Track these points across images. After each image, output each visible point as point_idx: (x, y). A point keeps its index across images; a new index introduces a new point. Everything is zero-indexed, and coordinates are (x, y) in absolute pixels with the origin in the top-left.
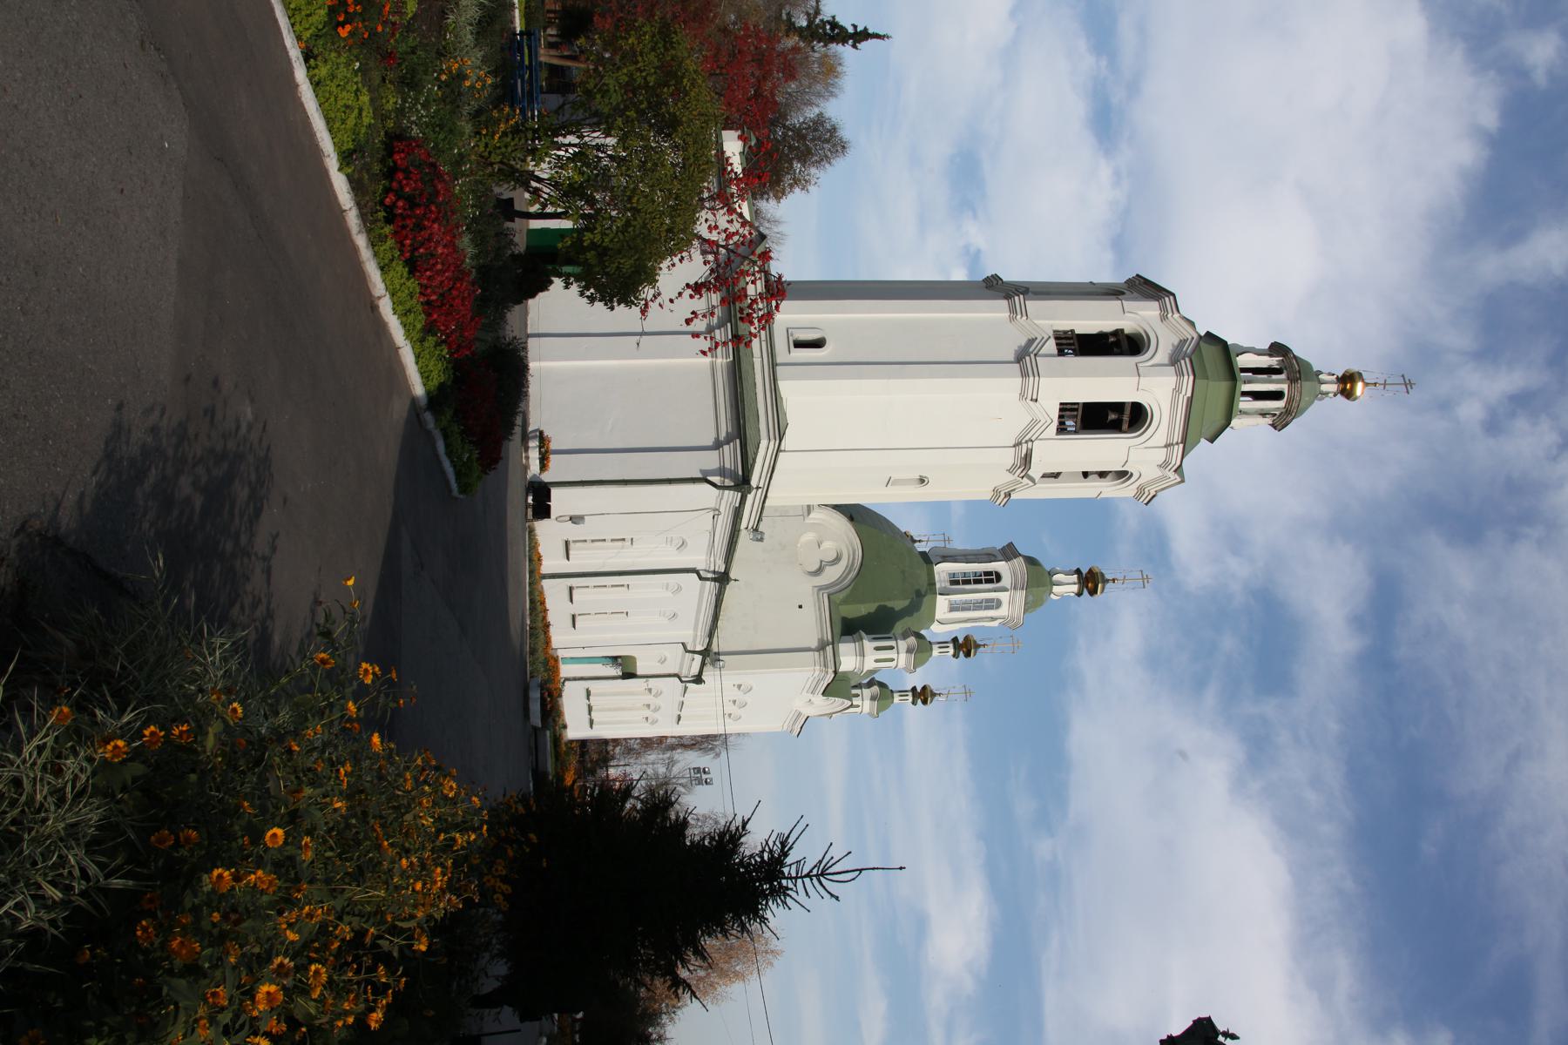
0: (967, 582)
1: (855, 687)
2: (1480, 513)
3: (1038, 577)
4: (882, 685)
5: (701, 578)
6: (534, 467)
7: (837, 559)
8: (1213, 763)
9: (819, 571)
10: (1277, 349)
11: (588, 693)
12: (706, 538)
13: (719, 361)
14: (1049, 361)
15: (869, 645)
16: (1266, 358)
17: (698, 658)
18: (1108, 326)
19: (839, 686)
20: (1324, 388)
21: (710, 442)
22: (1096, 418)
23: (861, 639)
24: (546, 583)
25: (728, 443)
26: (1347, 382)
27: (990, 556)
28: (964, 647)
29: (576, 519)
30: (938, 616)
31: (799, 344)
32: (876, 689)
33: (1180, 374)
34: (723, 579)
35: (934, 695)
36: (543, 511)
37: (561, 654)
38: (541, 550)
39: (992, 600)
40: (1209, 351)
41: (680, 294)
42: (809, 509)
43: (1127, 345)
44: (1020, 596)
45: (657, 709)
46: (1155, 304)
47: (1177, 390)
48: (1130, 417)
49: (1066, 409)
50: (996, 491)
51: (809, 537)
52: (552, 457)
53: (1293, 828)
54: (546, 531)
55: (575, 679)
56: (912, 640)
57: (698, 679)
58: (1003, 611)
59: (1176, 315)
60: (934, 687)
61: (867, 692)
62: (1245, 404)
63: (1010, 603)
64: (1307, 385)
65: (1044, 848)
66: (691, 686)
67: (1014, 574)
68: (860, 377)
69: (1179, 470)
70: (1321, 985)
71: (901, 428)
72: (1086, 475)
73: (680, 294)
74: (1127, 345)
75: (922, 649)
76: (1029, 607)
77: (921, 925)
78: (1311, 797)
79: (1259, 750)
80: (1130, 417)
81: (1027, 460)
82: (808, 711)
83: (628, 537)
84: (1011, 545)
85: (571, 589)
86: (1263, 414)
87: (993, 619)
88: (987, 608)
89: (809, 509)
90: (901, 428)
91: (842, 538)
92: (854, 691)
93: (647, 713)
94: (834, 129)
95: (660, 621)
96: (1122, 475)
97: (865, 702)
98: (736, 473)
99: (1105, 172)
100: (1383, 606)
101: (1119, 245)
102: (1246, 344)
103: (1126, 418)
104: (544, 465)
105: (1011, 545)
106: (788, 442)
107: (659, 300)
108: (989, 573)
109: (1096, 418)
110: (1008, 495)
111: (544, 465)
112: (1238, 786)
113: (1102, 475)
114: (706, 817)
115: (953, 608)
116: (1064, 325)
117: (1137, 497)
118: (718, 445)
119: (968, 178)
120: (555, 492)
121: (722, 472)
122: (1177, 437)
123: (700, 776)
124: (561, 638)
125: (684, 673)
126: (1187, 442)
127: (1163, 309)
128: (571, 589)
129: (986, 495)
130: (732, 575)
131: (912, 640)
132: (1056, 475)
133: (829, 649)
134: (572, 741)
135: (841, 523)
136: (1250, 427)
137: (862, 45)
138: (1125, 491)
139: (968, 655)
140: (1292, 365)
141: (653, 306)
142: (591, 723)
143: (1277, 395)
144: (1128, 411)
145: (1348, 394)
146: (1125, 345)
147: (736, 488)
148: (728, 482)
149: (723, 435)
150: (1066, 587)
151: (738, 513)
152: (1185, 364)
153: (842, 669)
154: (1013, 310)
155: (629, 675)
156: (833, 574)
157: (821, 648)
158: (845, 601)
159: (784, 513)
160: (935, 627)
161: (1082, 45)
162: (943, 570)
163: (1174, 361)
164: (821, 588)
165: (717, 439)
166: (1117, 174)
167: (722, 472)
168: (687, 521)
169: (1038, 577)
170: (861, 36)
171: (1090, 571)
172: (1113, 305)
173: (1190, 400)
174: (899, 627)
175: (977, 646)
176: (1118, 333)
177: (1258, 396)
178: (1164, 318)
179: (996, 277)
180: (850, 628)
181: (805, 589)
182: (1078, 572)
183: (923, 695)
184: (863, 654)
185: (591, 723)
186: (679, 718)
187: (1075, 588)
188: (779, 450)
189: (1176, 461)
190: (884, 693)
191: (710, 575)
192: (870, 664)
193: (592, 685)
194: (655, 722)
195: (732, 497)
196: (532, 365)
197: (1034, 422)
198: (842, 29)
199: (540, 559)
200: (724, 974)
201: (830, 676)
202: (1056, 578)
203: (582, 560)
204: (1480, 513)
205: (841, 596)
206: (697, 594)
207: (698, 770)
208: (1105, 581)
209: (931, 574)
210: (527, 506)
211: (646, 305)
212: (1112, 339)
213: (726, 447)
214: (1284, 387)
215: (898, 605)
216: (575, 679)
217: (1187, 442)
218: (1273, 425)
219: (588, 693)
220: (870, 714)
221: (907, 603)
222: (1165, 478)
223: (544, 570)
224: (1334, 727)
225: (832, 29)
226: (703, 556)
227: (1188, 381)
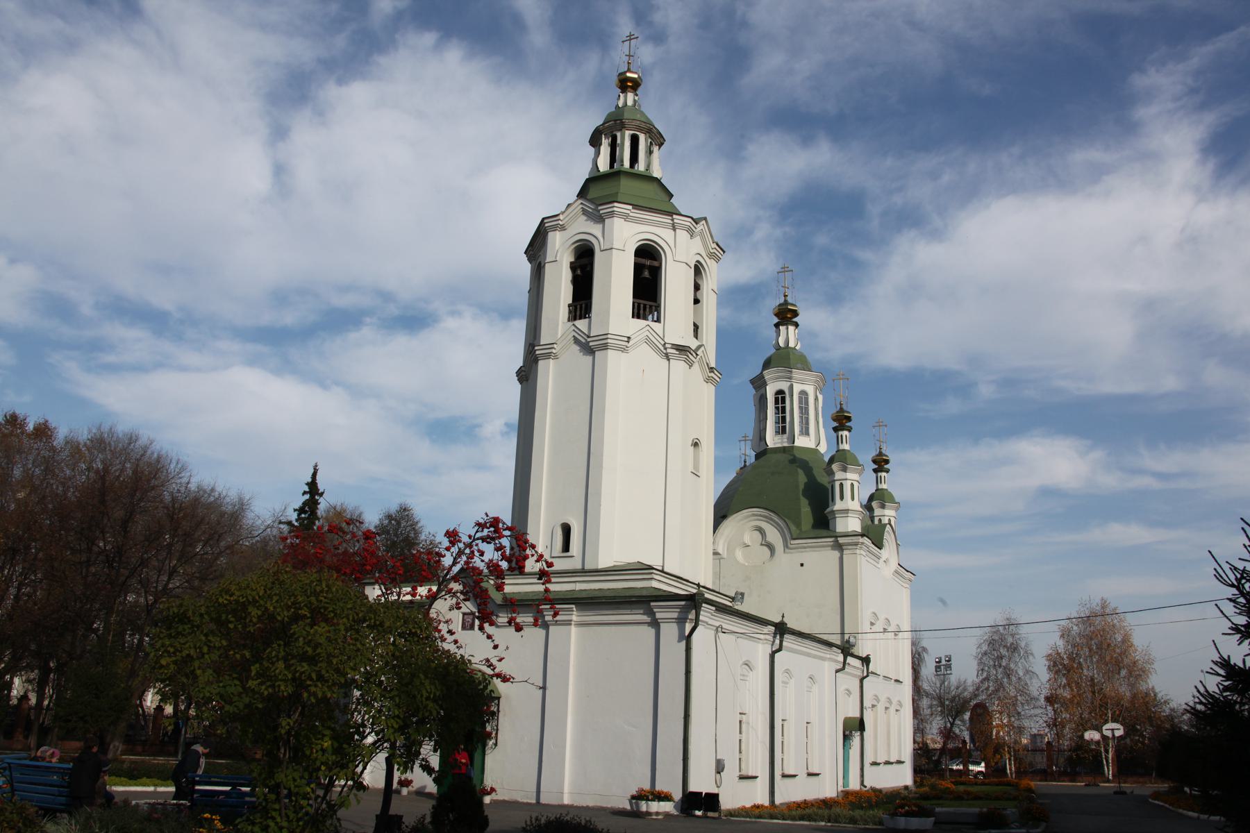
0: (784, 419)
1: (873, 521)
2: (725, 52)
3: (782, 359)
4: (871, 498)
5: (780, 649)
6: (667, 807)
7: (761, 531)
8: (917, 256)
9: (771, 548)
10: (595, 141)
11: (875, 764)
12: (744, 642)
13: (574, 618)
14: (593, 326)
15: (839, 505)
16: (602, 148)
17: (850, 660)
18: (566, 276)
19: (874, 534)
20: (630, 103)
22: (647, 293)
23: (833, 512)
24: (777, 802)
26: (626, 85)
27: (762, 401)
28: (841, 421)
29: (720, 767)
30: (813, 446)
31: (566, 547)
32: (874, 504)
33: (612, 214)
34: (781, 629)
35: (880, 454)
36: (711, 801)
37: (840, 788)
38: (748, 805)
39: (800, 399)
41: (489, 637)
42: (715, 553)
43: (584, 261)
44: (797, 374)
45: (889, 701)
46: (550, 235)
47: (626, 217)
48: (648, 265)
49: (638, 313)
50: (708, 380)
51: (739, 554)
52: (658, 788)
53: (970, 193)
54: (734, 797)
55: (862, 776)
56: (835, 467)
57: (866, 661)
58: (810, 389)
59: (561, 217)
60: (874, 453)
61: (877, 512)
62: (641, 167)
63: (803, 384)
64: (626, 115)
65: (986, 391)
66: (871, 668)
67: (778, 379)
68: (599, 494)
69: (696, 221)
70: (1097, 173)
71: (645, 468)
72: (696, 301)
73: (489, 637)
74: (584, 261)
75: (842, 458)
76: (806, 366)
77: (1047, 492)
78: (946, 178)
79: (909, 219)
80: (648, 265)
81: (682, 349)
82: (893, 565)
83: (738, 717)
84: (752, 382)
85: (784, 776)
86: (650, 152)
87: (816, 399)
88: (807, 403)
89: (715, 553)
90: (645, 468)
91: (742, 525)
92: (876, 522)
93: (892, 710)
94: (389, 517)
95: (815, 692)
96: (698, 270)
97: (887, 514)
99: (451, 323)
100: (796, 121)
101: (506, 315)
102: (590, 166)
103: (648, 263)
104: (664, 797)
105: (752, 382)
106: (657, 563)
107: (494, 661)
108: (777, 401)
109: (647, 293)
111: (664, 797)
112: (936, 235)
113: (697, 287)
114: (980, 663)
115: (805, 432)
116: (564, 312)
117: (718, 260)
118: (655, 624)
119: (448, 430)
120: (693, 787)
121: (681, 621)
122: (667, 219)
123: (944, 666)
124: (827, 789)
125: (859, 673)
126: (672, 212)
127: (554, 228)
128: (784, 776)
129: (710, 390)
130: (777, 620)
131: (835, 467)
132: (696, 327)
133: (841, 540)
134: (915, 782)
135: (729, 525)
136: (657, 164)
137: (321, 488)
138: (711, 267)
139: (849, 419)
141: (500, 667)
142: (899, 762)
143: (635, 141)
144: (642, 261)
145: (635, 85)
146: (584, 261)
147: (698, 609)
148: (692, 615)
149: (645, 618)
150: (790, 336)
151: (721, 609)
152: (604, 210)
153: (859, 530)
154: (548, 356)
155: (861, 726)
156: (774, 535)
157: (839, 547)
158: (798, 525)
159: (718, 575)
160: (823, 448)
161: (353, 336)
162: (772, 440)
163: (600, 219)
164: (786, 546)
165: (649, 624)
166: (453, 313)
167: (681, 621)
168: (725, 659)
169: (782, 359)
170: (313, 488)
171: (776, 315)
172: (549, 270)
173: (635, 207)
174: (823, 479)
175: (841, 410)
176: (573, 267)
177: (634, 158)
178: (563, 228)
179: (519, 373)
180: (822, 522)
181: (786, 560)
182: (777, 325)
183: (881, 464)
184: (847, 511)
185: (899, 762)
187: (791, 328)
188: (662, 571)
189: (688, 222)
190: (879, 497)
191: (777, 642)
192: (855, 505)
193: (867, 761)
194: (900, 704)
195: (706, 613)
196: (566, 801)
197: (648, 341)
198: (305, 504)
199: (757, 807)
200: (1124, 653)
201: (866, 540)
202: (782, 344)
203: (758, 765)
204: (725, 52)
205: (793, 528)
206: (793, 657)
207: (938, 668)
208: (786, 303)
209: (776, 450)
210: (705, 817)
211: (498, 675)
213: (658, 616)
214: (628, 133)
215: (802, 479)
216: (862, 776)
217: (672, 212)
218: (660, 145)
219: (875, 764)
220: (897, 509)
221: (800, 471)
222: (702, 232)
223: (765, 801)
224: (889, 162)
225: (305, 512)
226: (759, 647)
227: (619, 207)
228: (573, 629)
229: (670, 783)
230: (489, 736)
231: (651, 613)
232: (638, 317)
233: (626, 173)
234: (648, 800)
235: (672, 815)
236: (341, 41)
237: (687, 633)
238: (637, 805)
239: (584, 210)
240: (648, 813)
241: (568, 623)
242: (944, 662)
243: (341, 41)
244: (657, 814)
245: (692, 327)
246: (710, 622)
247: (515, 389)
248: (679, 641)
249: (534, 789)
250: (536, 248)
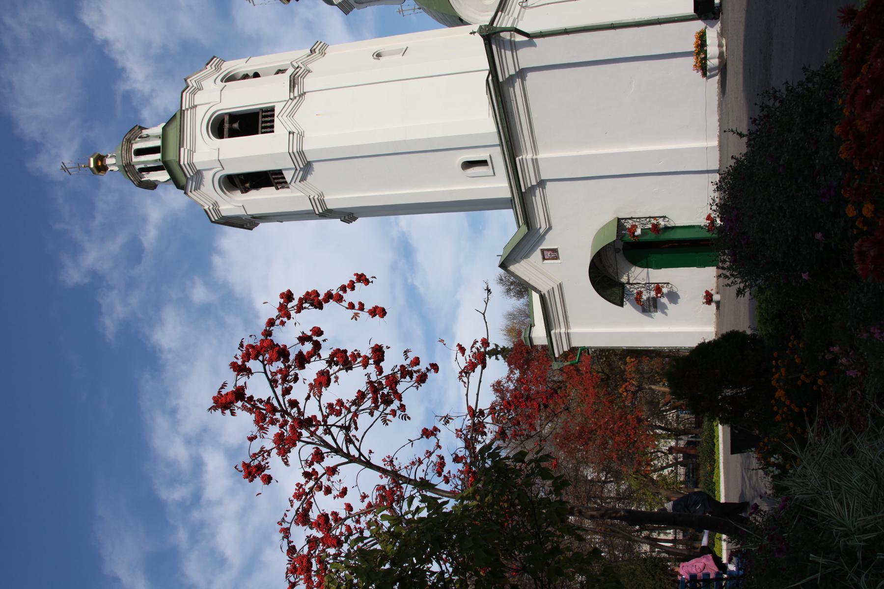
13: (529, 156)
16: (152, 179)
21: (530, 76)
25: (511, 77)
31: (483, 163)
33: (191, 165)
40: (183, 180)
46: (224, 214)
47: (192, 152)
49: (270, 129)
50: (323, 53)
52: (692, 48)
59: (206, 207)
62: (158, 143)
72: (256, 75)
81: (293, 83)
98: (499, 47)
103: (227, 125)
104: (702, 38)
110: (312, 51)
111: (702, 38)
113: (246, 77)
116: (283, 193)
118: (522, 74)
122: (188, 115)
127: (217, 211)
140: (133, 175)
143: (140, 152)
146: (237, 181)
148: (506, 35)
149: (518, 84)
152: (189, 173)
154: (322, 202)
161: (422, 290)
163: (199, 174)
165: (523, 80)
167: (514, 46)
172: (252, 211)
173: (181, 145)
176: (245, 190)
178: (215, 204)
195: (504, 21)
196: (715, 143)
197: (291, 115)
212: (248, 185)
213: (512, 72)
214: (135, 159)
227: (184, 161)
228: (541, 156)
229: (685, 36)
230: (655, 227)
231: (511, 79)
232: (273, 127)
233: (163, 156)
234: (705, 58)
235: (722, 29)
236: (230, 320)
237: (526, 39)
238: (712, 69)
239: (196, 189)
240: (721, 55)
241: (535, 162)
243: (230, 320)
244: (720, 45)
245: (280, 75)
246: (515, 15)
247: (262, 226)
248: (535, 45)
249: (706, 175)
250: (247, 223)
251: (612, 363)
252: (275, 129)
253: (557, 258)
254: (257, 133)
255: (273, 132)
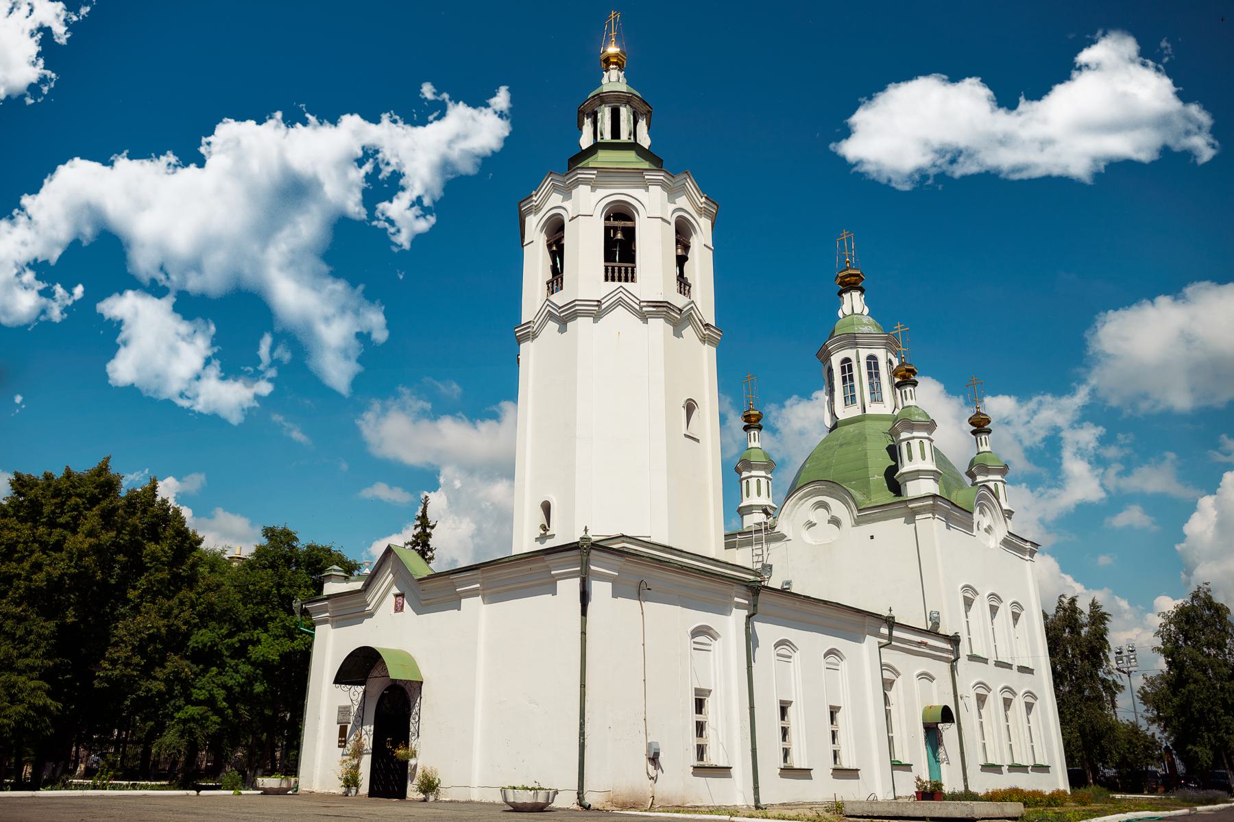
16: (585, 128)
49: (610, 276)
59: (535, 198)
62: (624, 137)
91: (200, 536)
108: (843, 369)
116: (542, 289)
127: (529, 211)
144: (613, 223)
177: (616, 132)
186: (700, 705)
187: (856, 294)
242: (1125, 653)
251: (295, 671)
252: (610, 283)
253: (396, 611)
254: (606, 261)
255: (606, 280)
